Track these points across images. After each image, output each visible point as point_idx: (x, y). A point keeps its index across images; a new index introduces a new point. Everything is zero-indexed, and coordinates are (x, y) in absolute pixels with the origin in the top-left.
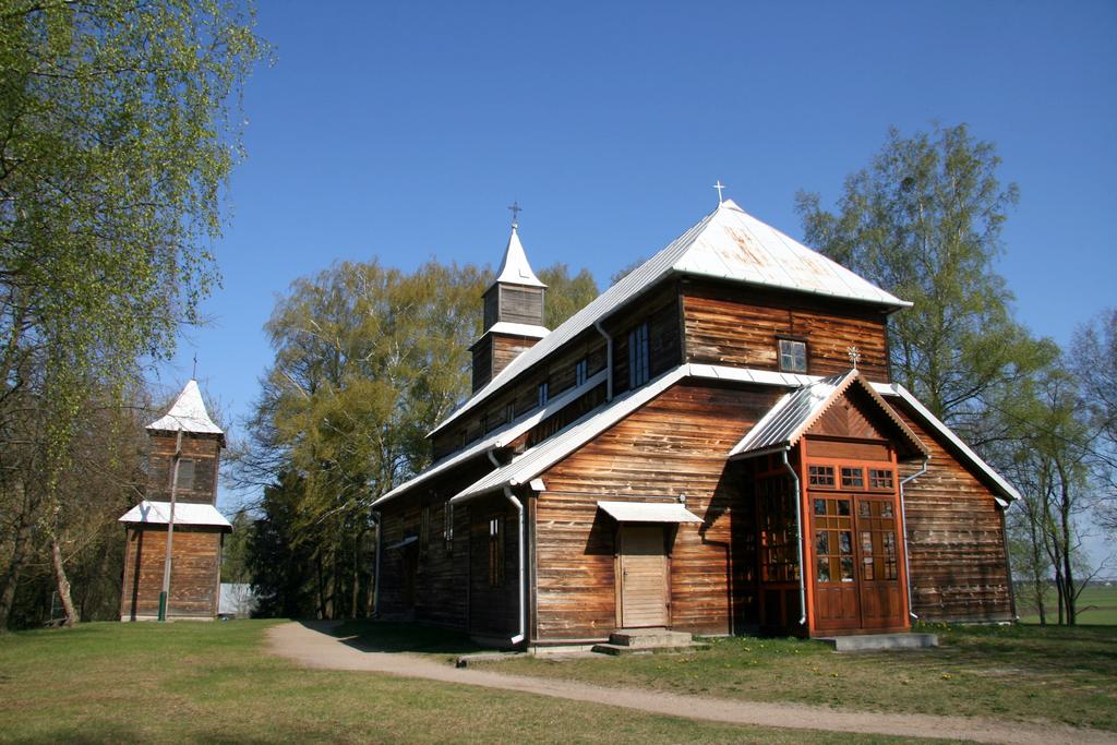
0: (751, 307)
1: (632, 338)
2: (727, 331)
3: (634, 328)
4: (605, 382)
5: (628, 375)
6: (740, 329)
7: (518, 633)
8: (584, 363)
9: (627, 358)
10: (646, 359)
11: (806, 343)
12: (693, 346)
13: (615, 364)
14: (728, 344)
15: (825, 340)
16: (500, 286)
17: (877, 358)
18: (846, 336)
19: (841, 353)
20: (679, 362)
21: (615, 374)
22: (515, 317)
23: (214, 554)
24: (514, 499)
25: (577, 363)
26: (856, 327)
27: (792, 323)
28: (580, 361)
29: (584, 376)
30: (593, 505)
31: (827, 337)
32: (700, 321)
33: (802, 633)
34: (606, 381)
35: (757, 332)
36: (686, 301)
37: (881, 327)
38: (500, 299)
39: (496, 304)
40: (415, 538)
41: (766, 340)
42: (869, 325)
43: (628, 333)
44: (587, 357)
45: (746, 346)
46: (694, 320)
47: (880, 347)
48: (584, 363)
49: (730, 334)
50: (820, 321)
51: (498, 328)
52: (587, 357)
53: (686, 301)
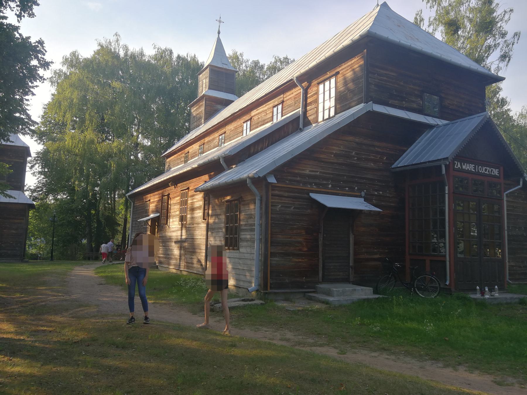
8: (280, 107)
30: (306, 196)
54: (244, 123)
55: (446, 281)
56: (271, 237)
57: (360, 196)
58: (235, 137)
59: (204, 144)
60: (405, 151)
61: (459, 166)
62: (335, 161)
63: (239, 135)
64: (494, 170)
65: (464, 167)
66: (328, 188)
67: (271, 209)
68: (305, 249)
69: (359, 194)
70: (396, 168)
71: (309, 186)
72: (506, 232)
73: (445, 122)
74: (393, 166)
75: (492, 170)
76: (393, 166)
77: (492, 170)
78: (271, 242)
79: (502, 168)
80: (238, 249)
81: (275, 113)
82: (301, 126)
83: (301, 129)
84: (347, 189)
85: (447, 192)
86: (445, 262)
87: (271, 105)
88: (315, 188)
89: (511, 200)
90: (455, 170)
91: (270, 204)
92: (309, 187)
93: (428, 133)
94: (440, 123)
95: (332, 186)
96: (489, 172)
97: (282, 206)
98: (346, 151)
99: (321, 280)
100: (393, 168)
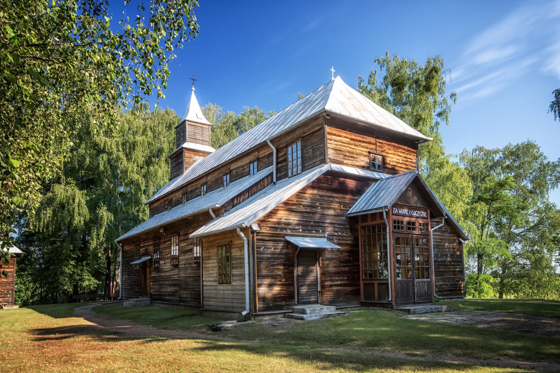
0: (356, 134)
1: (290, 149)
2: (347, 147)
3: (292, 143)
4: (271, 174)
5: (287, 169)
6: (353, 147)
7: (244, 309)
8: (256, 163)
9: (286, 160)
10: (300, 160)
11: (382, 156)
12: (330, 153)
13: (278, 163)
14: (348, 154)
15: (391, 156)
16: (187, 122)
17: (413, 167)
18: (400, 154)
19: (398, 163)
20: (323, 161)
21: (278, 170)
22: (195, 140)
23: (12, 270)
24: (242, 235)
25: (250, 163)
26: (405, 149)
27: (376, 145)
28: (253, 162)
29: (256, 170)
30: (283, 239)
31: (392, 154)
32: (334, 141)
33: (388, 306)
34: (272, 173)
35: (360, 148)
36: (328, 129)
37: (415, 151)
38: (187, 130)
39: (184, 131)
40: (149, 257)
41: (365, 153)
42: (410, 149)
43: (287, 146)
44: (258, 159)
45: (355, 156)
46: (331, 140)
47: (414, 161)
48: (256, 163)
49: (348, 149)
50: (388, 145)
51: (185, 145)
52: (258, 159)
53: (328, 129)
54: (224, 175)
55: (389, 298)
56: (258, 272)
57: (324, 237)
58: (216, 187)
59: (186, 193)
60: (357, 200)
61: (396, 211)
62: (304, 210)
63: (220, 186)
64: (423, 212)
65: (400, 212)
66: (299, 232)
67: (257, 251)
68: (284, 280)
69: (324, 235)
70: (351, 214)
71: (285, 231)
72: (433, 259)
73: (387, 176)
74: (348, 212)
75: (421, 213)
76: (348, 212)
77: (421, 213)
78: (258, 276)
79: (429, 211)
80: (230, 283)
81: (252, 168)
82: (275, 180)
83: (274, 183)
84: (314, 232)
85: (388, 231)
86: (388, 284)
87: (248, 161)
88: (289, 232)
89: (440, 234)
90: (393, 214)
91: (256, 247)
92: (284, 232)
93: (375, 185)
94: (383, 177)
95: (303, 230)
96: (419, 214)
97: (264, 248)
98: (312, 203)
99: (296, 303)
100: (349, 214)
